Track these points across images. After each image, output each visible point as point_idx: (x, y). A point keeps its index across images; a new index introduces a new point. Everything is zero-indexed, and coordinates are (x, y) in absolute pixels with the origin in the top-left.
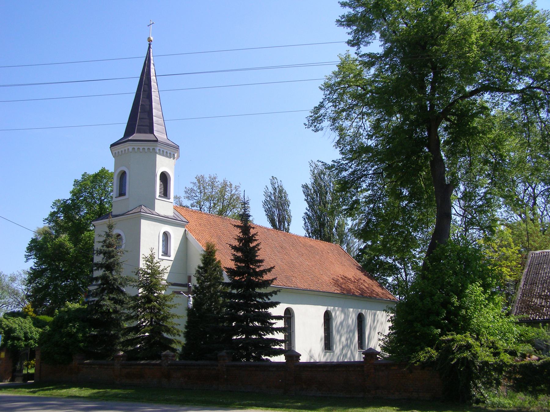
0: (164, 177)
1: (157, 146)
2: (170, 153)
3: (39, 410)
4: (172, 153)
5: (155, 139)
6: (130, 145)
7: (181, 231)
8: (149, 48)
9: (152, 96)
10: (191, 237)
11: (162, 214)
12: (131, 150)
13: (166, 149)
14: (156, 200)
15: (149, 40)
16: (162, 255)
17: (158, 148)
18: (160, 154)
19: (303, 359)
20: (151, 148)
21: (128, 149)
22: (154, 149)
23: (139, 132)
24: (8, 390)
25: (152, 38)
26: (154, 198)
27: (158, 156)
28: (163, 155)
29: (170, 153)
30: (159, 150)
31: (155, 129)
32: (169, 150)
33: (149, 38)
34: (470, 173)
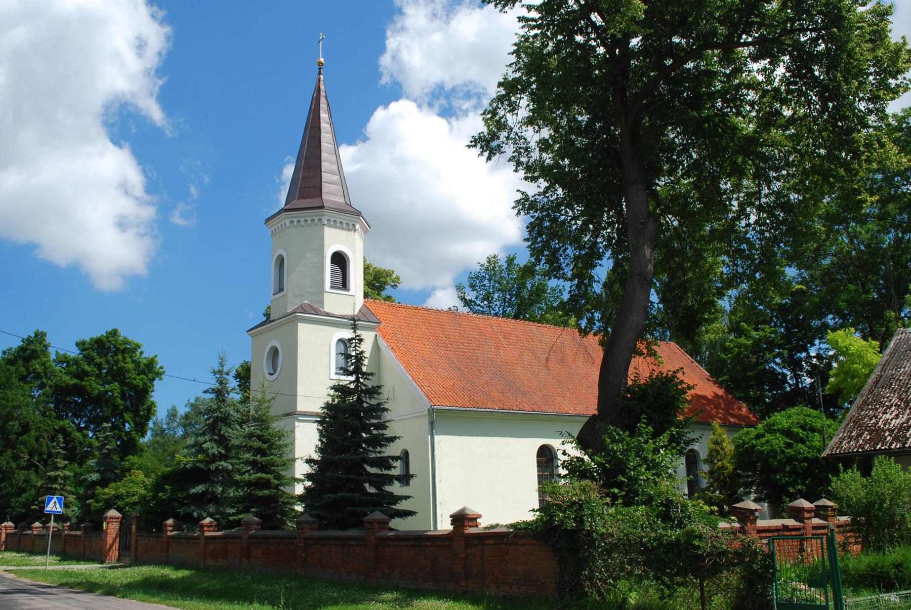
0: (340, 260)
1: (323, 215)
3: (310, 412)
4: (351, 223)
5: (321, 205)
6: (288, 218)
7: (373, 334)
9: (323, 144)
10: (382, 343)
11: (337, 313)
12: (288, 224)
13: (339, 217)
14: (325, 294)
16: (336, 374)
17: (326, 218)
18: (330, 226)
19: (596, 412)
21: (285, 223)
22: (320, 220)
24: (116, 537)
26: (322, 291)
27: (326, 229)
30: (328, 220)
31: (324, 190)
32: (346, 218)
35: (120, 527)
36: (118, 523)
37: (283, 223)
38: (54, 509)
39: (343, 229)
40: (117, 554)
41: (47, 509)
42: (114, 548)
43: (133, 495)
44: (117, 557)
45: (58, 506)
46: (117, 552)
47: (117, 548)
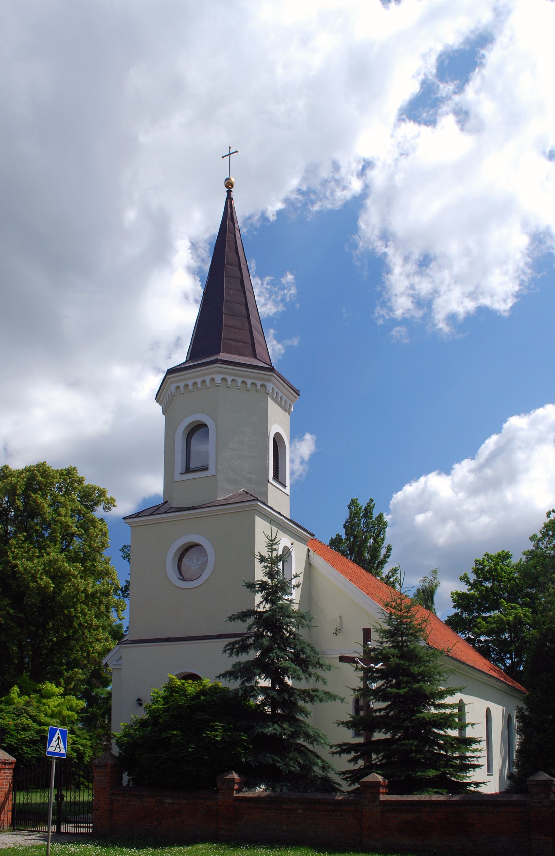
1: (269, 381)
2: (281, 398)
6: (220, 373)
8: (229, 198)
15: (229, 185)
20: (259, 383)
21: (213, 380)
23: (225, 352)
25: (233, 179)
28: (276, 402)
29: (281, 398)
30: (273, 390)
33: (228, 179)
34: (10, 549)
35: (13, 777)
36: (11, 771)
37: (207, 379)
38: (57, 750)
39: (281, 406)
40: (10, 817)
41: (50, 749)
42: (6, 808)
43: (24, 729)
44: (10, 821)
45: (62, 745)
46: (10, 813)
47: (10, 807)
